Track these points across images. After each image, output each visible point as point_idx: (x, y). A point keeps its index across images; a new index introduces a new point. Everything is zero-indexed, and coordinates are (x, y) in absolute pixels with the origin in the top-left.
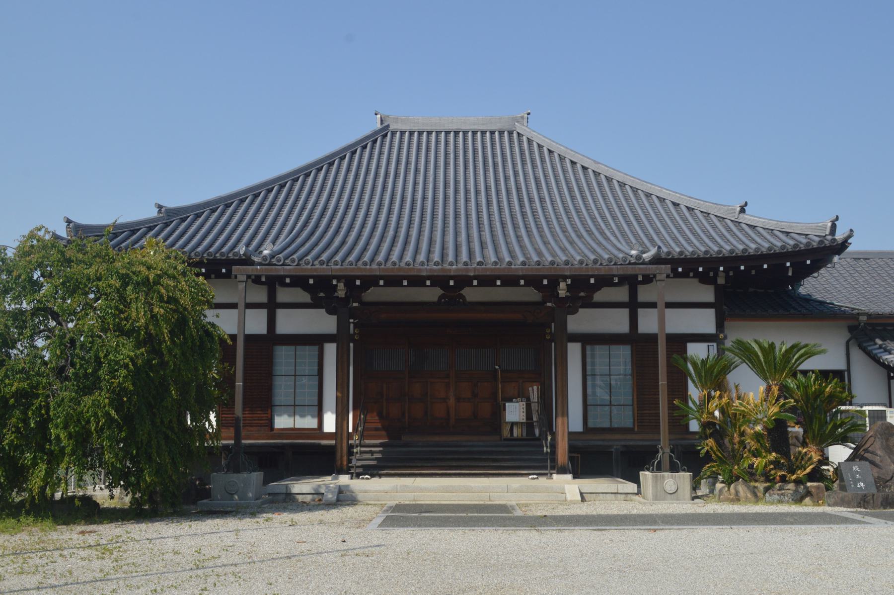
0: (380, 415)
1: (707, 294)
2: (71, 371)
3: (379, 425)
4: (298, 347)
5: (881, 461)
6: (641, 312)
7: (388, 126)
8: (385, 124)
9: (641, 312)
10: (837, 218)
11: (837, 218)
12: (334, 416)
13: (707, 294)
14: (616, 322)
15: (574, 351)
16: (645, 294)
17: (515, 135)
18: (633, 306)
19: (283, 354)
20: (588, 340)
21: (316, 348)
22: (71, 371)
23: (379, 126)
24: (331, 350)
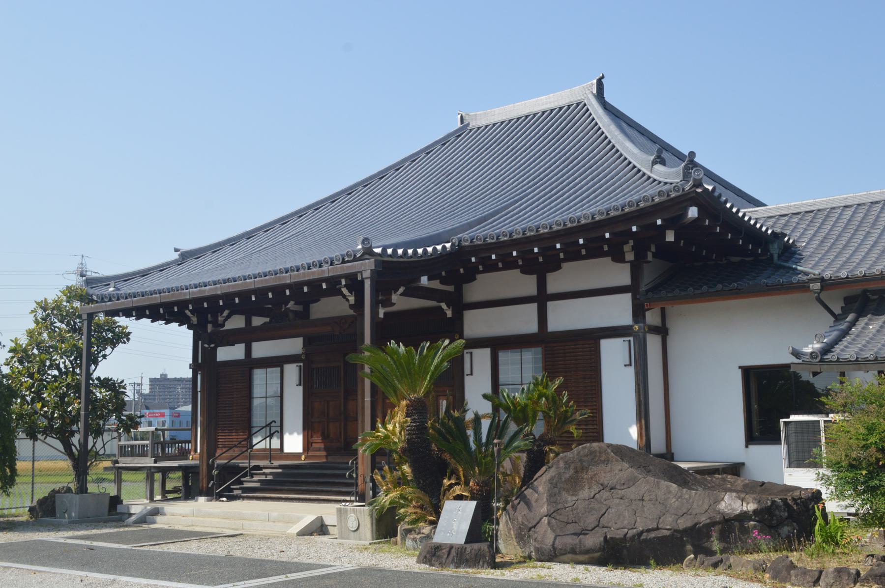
0: (323, 435)
1: (621, 275)
2: (39, 405)
3: (322, 446)
4: (268, 370)
5: (536, 501)
6: (550, 305)
7: (468, 124)
8: (466, 122)
9: (550, 305)
10: (603, 77)
11: (603, 77)
12: (301, 437)
13: (621, 275)
14: (522, 319)
15: (482, 358)
16: (556, 283)
17: (596, 127)
18: (542, 299)
19: (259, 375)
20: (497, 345)
21: (279, 369)
22: (39, 405)
23: (459, 125)
24: (292, 371)
